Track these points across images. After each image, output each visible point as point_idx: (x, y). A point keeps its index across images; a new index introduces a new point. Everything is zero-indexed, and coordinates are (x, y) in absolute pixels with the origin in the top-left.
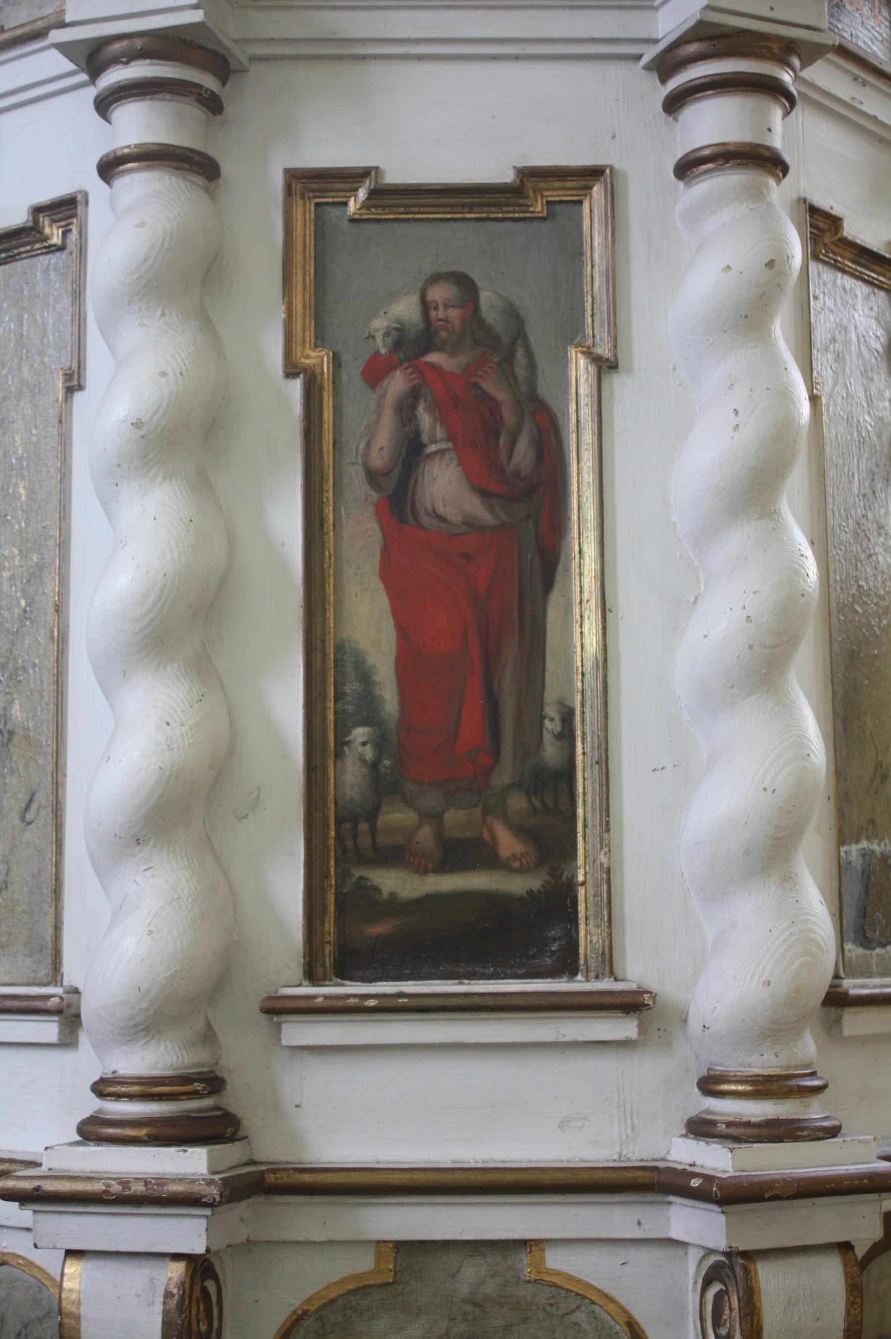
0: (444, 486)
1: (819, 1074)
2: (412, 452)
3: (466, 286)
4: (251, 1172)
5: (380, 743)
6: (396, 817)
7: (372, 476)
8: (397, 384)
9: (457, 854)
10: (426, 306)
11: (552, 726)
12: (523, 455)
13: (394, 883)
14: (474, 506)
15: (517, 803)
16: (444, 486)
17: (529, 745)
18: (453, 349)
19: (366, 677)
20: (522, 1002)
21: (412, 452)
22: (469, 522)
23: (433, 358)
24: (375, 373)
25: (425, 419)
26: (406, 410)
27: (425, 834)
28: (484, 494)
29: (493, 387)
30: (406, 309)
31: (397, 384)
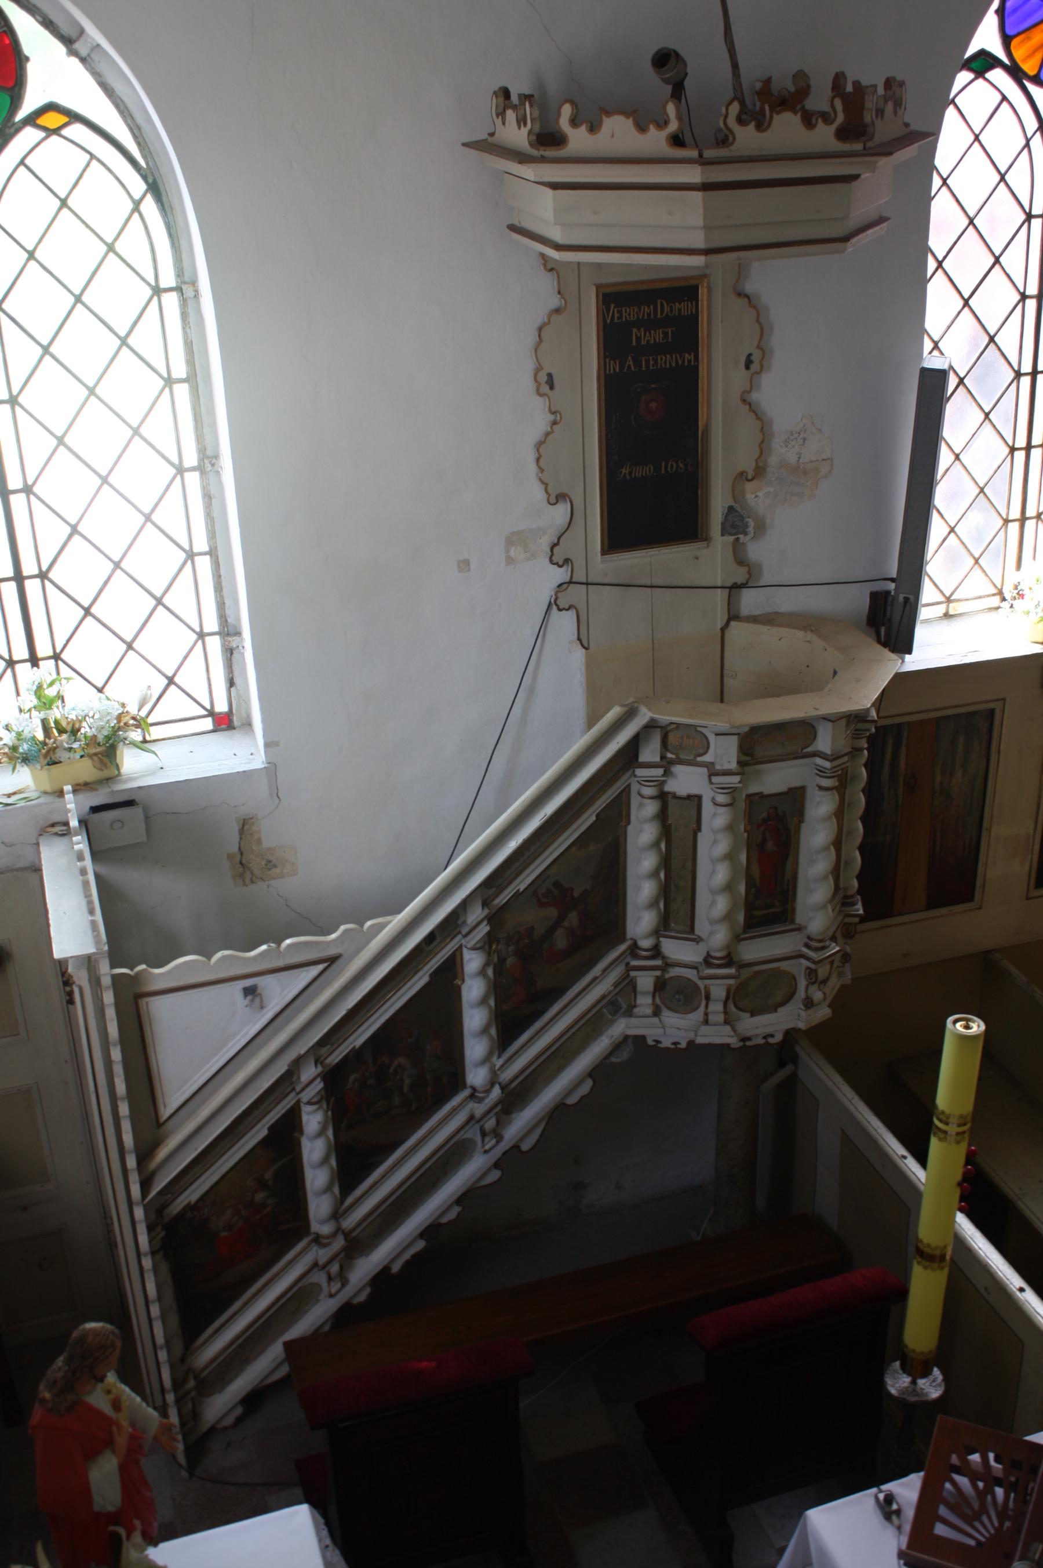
0: (770, 845)
2: (764, 840)
16: (770, 845)
21: (764, 840)
30: (765, 815)
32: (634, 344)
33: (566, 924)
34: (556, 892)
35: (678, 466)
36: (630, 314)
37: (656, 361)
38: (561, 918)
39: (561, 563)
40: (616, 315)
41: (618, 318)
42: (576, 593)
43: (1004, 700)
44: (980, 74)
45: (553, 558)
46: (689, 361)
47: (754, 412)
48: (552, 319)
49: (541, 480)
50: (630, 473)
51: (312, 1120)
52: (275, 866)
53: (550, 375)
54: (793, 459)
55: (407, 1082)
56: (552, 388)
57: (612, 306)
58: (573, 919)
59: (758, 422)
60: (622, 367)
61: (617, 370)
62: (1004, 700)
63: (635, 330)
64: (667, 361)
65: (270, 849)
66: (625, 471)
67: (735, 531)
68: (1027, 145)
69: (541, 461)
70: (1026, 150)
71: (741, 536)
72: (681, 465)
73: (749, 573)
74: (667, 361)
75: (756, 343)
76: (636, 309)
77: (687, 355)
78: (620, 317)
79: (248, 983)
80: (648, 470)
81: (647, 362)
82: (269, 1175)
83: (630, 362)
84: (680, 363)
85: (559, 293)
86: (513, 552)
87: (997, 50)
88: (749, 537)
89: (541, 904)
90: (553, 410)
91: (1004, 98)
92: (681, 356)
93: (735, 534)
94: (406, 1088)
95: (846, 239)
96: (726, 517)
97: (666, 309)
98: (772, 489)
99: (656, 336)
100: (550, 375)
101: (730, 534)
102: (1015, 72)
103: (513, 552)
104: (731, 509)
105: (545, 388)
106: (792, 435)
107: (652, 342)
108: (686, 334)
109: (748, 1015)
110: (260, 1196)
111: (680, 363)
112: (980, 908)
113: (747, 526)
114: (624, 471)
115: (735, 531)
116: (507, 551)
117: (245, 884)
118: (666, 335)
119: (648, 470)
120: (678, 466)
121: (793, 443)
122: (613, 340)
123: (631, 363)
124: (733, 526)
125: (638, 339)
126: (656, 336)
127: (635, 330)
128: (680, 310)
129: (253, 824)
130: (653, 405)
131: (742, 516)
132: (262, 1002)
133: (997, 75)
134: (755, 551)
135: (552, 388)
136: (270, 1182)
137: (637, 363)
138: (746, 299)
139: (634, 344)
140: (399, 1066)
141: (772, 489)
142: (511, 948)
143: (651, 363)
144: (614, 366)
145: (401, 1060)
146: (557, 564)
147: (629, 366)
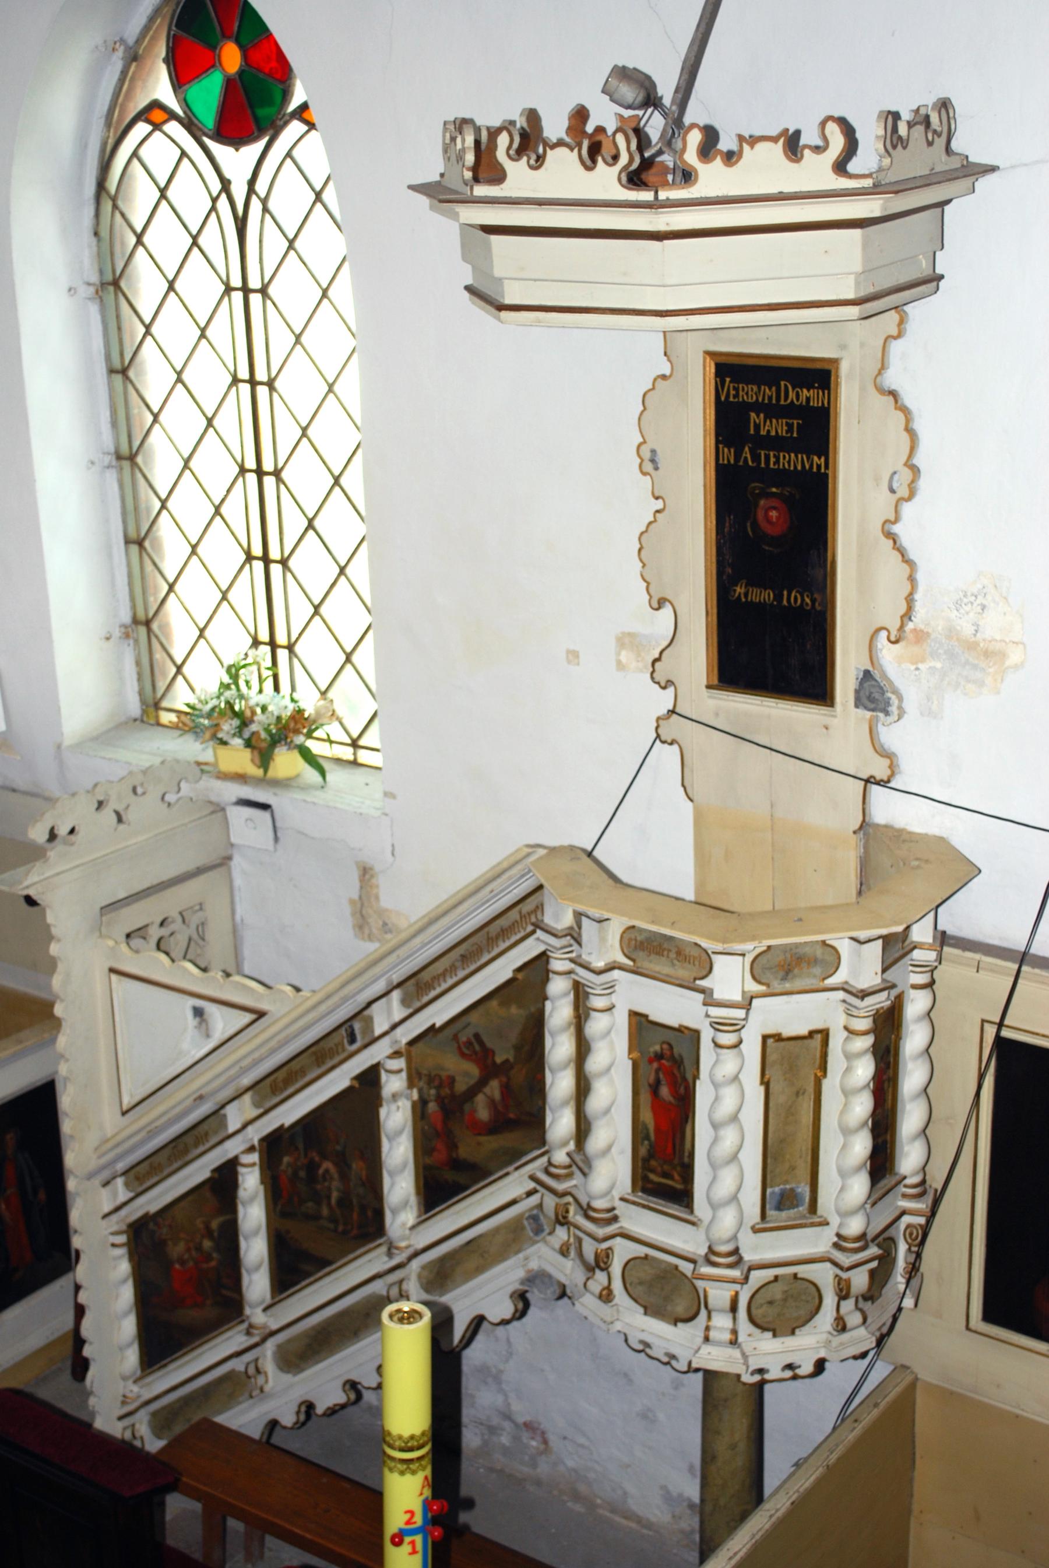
0: (665, 1091)
1: (122, 827)
2: (658, 1083)
3: (671, 1047)
4: (289, 1341)
5: (650, 1145)
6: (653, 1163)
7: (650, 1085)
8: (655, 1065)
9: (666, 1175)
10: (662, 1049)
11: (686, 1154)
12: (682, 1090)
13: (652, 1177)
14: (671, 1099)
15: (679, 1169)
16: (665, 1091)
17: (681, 1157)
18: (668, 1061)
19: (647, 1129)
20: (863, 191)
21: (658, 1083)
22: (670, 1102)
23: (663, 1061)
24: (651, 1061)
25: (661, 1076)
26: (657, 1071)
27: (659, 1169)
28: (674, 1097)
29: (676, 1072)
30: (657, 1048)
31: (655, 1065)
32: (752, 432)
33: (487, 1090)
34: (477, 1047)
35: (803, 600)
36: (749, 393)
37: (777, 458)
38: (482, 1083)
39: (663, 684)
40: (732, 392)
41: (735, 397)
42: (674, 728)
43: (983, 1021)
44: (157, 127)
45: (655, 675)
46: (819, 467)
47: (898, 550)
48: (656, 384)
49: (642, 576)
50: (746, 595)
51: (250, 1182)
52: (391, 931)
53: (653, 452)
54: (967, 630)
55: (335, 1195)
56: (656, 469)
57: (728, 380)
58: (494, 1088)
59: (905, 566)
60: (737, 457)
61: (732, 462)
62: (983, 1021)
63: (753, 415)
64: (791, 461)
65: (387, 910)
66: (740, 590)
67: (872, 706)
68: (213, 208)
69: (643, 552)
70: (267, 216)
71: (881, 715)
72: (808, 600)
73: (891, 767)
74: (791, 461)
75: (905, 458)
76: (755, 388)
77: (816, 458)
78: (736, 396)
79: (199, 1003)
80: (766, 596)
81: (767, 457)
82: (215, 1224)
83: (747, 453)
84: (807, 467)
85: (665, 354)
86: (624, 656)
87: (170, 100)
88: (889, 719)
89: (463, 1055)
90: (657, 494)
91: (184, 154)
92: (808, 459)
93: (873, 710)
94: (333, 1201)
95: (502, 308)
96: (862, 682)
97: (792, 395)
98: (939, 665)
99: (777, 427)
100: (653, 452)
101: (866, 708)
102: (191, 125)
103: (624, 656)
104: (867, 674)
105: (648, 467)
106: (965, 596)
107: (773, 433)
108: (816, 430)
109: (641, 1310)
110: (207, 1244)
111: (807, 467)
112: (968, 1328)
113: (888, 703)
114: (738, 589)
115: (872, 706)
116: (618, 654)
117: (363, 939)
118: (790, 427)
119: (766, 596)
120: (803, 600)
121: (968, 608)
122: (729, 423)
123: (748, 456)
124: (871, 699)
125: (757, 427)
126: (777, 427)
127: (753, 415)
128: (808, 399)
129: (372, 876)
130: (774, 514)
131: (881, 688)
132: (207, 1029)
133: (173, 128)
134: (891, 735)
135: (656, 469)
136: (216, 1234)
137: (756, 458)
138: (891, 398)
139: (752, 432)
140: (327, 1171)
141: (939, 665)
142: (433, 1092)
143: (772, 460)
144: (728, 455)
145: (327, 1165)
146: (658, 683)
147: (746, 458)
